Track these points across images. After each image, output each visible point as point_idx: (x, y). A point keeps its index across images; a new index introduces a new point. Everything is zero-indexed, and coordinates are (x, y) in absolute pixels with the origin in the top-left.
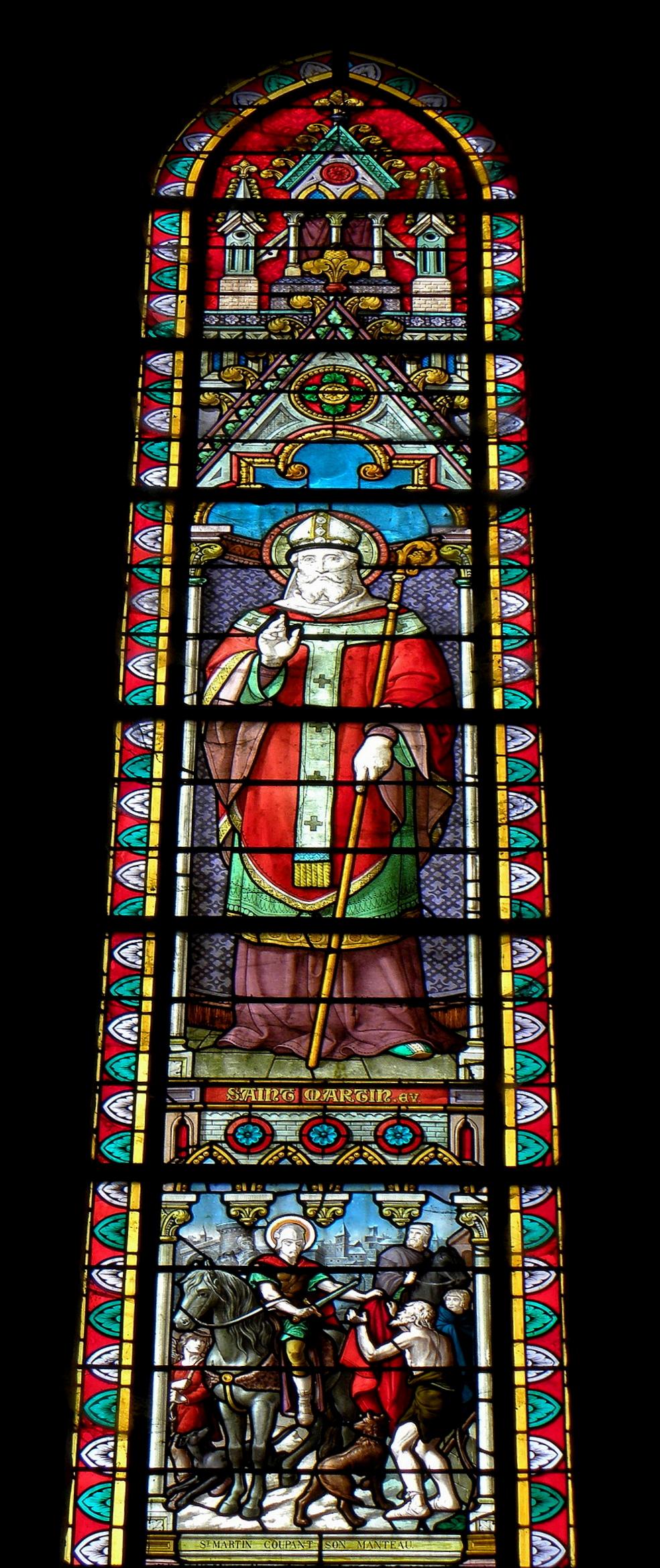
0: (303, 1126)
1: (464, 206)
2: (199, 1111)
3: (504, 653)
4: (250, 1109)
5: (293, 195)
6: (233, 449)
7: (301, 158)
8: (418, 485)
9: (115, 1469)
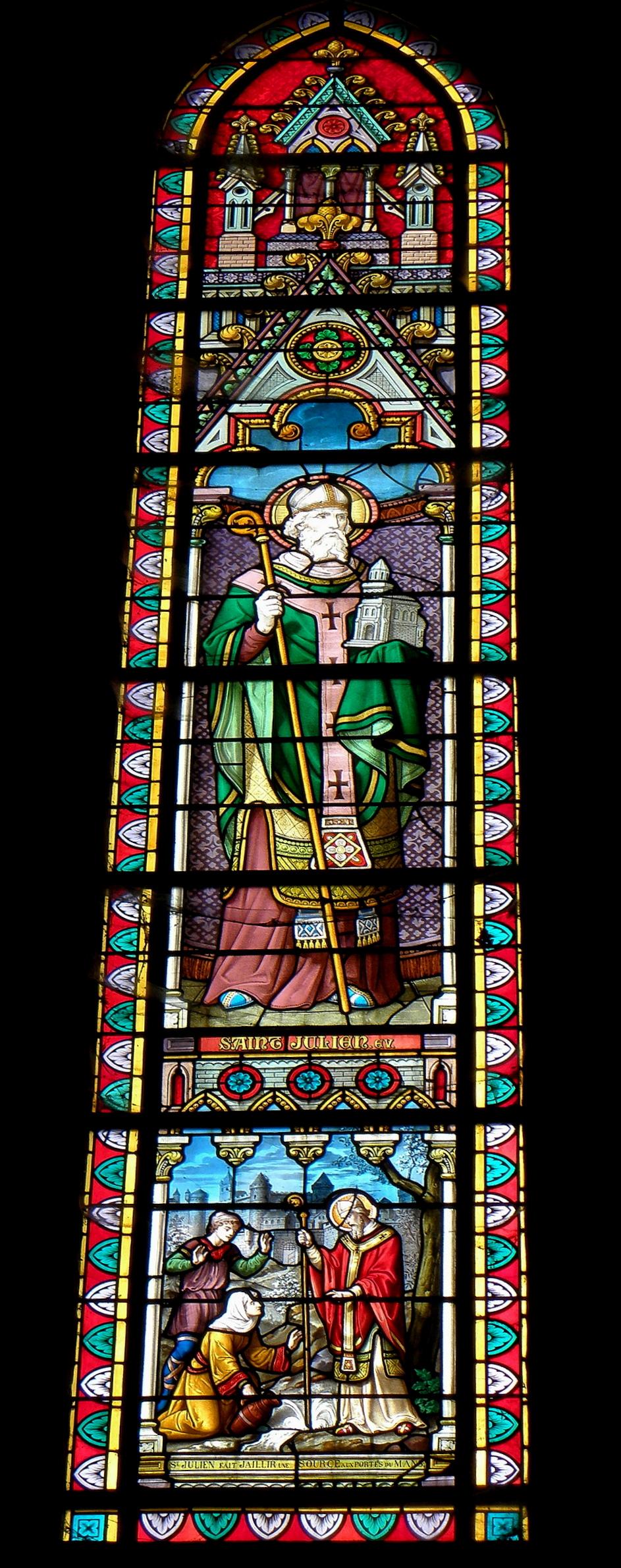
0: (290, 1074)
1: (453, 158)
2: (194, 1061)
3: (483, 607)
4: (242, 1058)
5: (291, 150)
6: (231, 410)
7: (298, 112)
8: (405, 444)
9: (153, 741)
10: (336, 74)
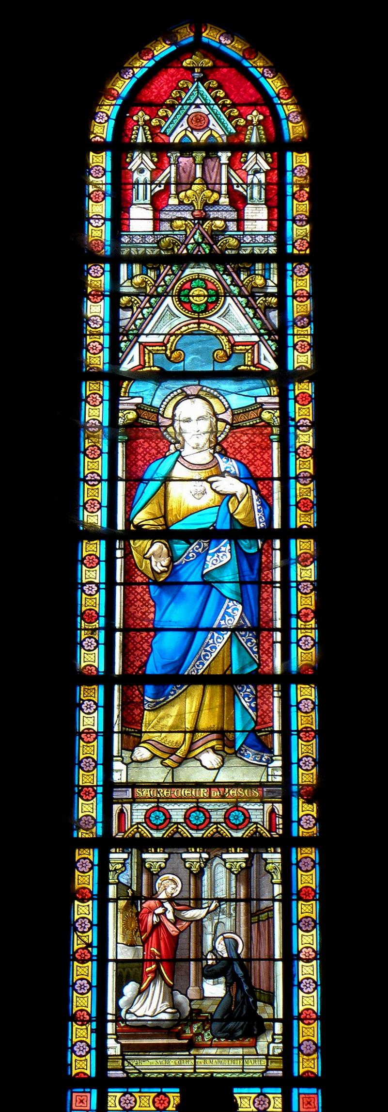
4: (158, 802)
7: (175, 109)
8: (248, 366)
10: (199, 80)
